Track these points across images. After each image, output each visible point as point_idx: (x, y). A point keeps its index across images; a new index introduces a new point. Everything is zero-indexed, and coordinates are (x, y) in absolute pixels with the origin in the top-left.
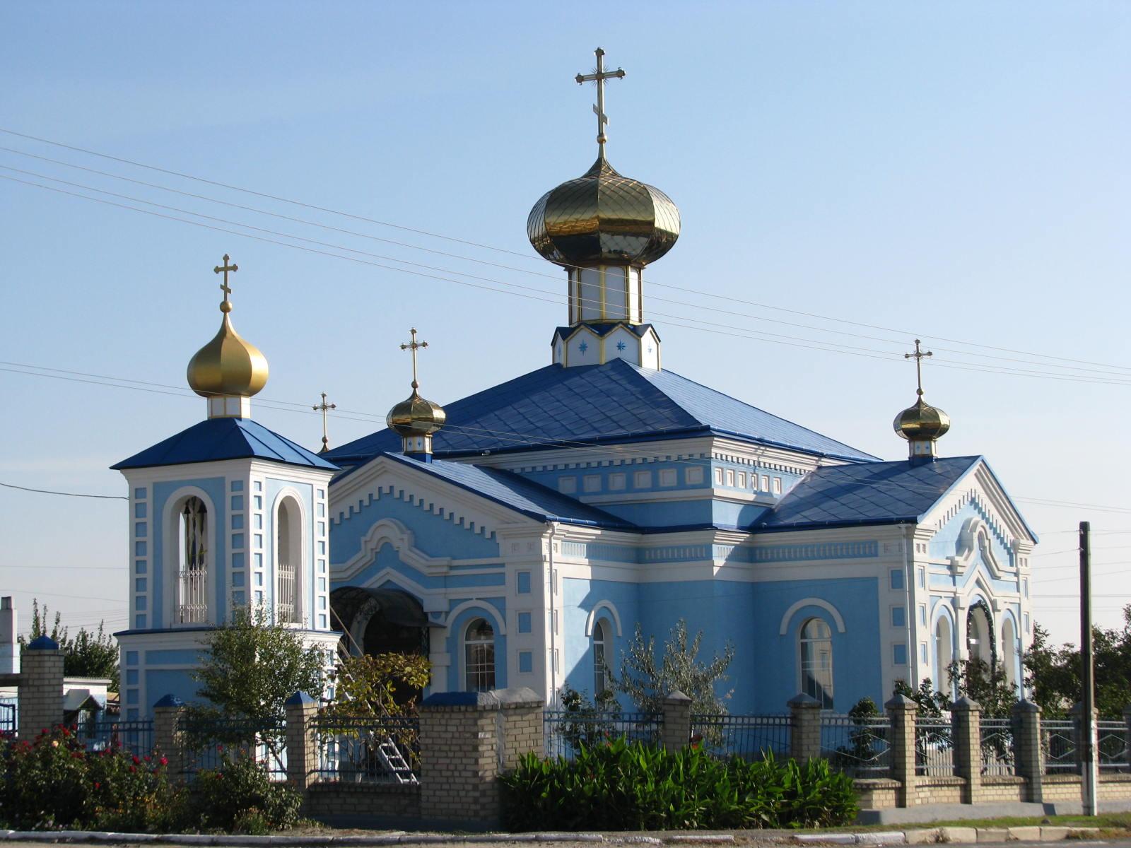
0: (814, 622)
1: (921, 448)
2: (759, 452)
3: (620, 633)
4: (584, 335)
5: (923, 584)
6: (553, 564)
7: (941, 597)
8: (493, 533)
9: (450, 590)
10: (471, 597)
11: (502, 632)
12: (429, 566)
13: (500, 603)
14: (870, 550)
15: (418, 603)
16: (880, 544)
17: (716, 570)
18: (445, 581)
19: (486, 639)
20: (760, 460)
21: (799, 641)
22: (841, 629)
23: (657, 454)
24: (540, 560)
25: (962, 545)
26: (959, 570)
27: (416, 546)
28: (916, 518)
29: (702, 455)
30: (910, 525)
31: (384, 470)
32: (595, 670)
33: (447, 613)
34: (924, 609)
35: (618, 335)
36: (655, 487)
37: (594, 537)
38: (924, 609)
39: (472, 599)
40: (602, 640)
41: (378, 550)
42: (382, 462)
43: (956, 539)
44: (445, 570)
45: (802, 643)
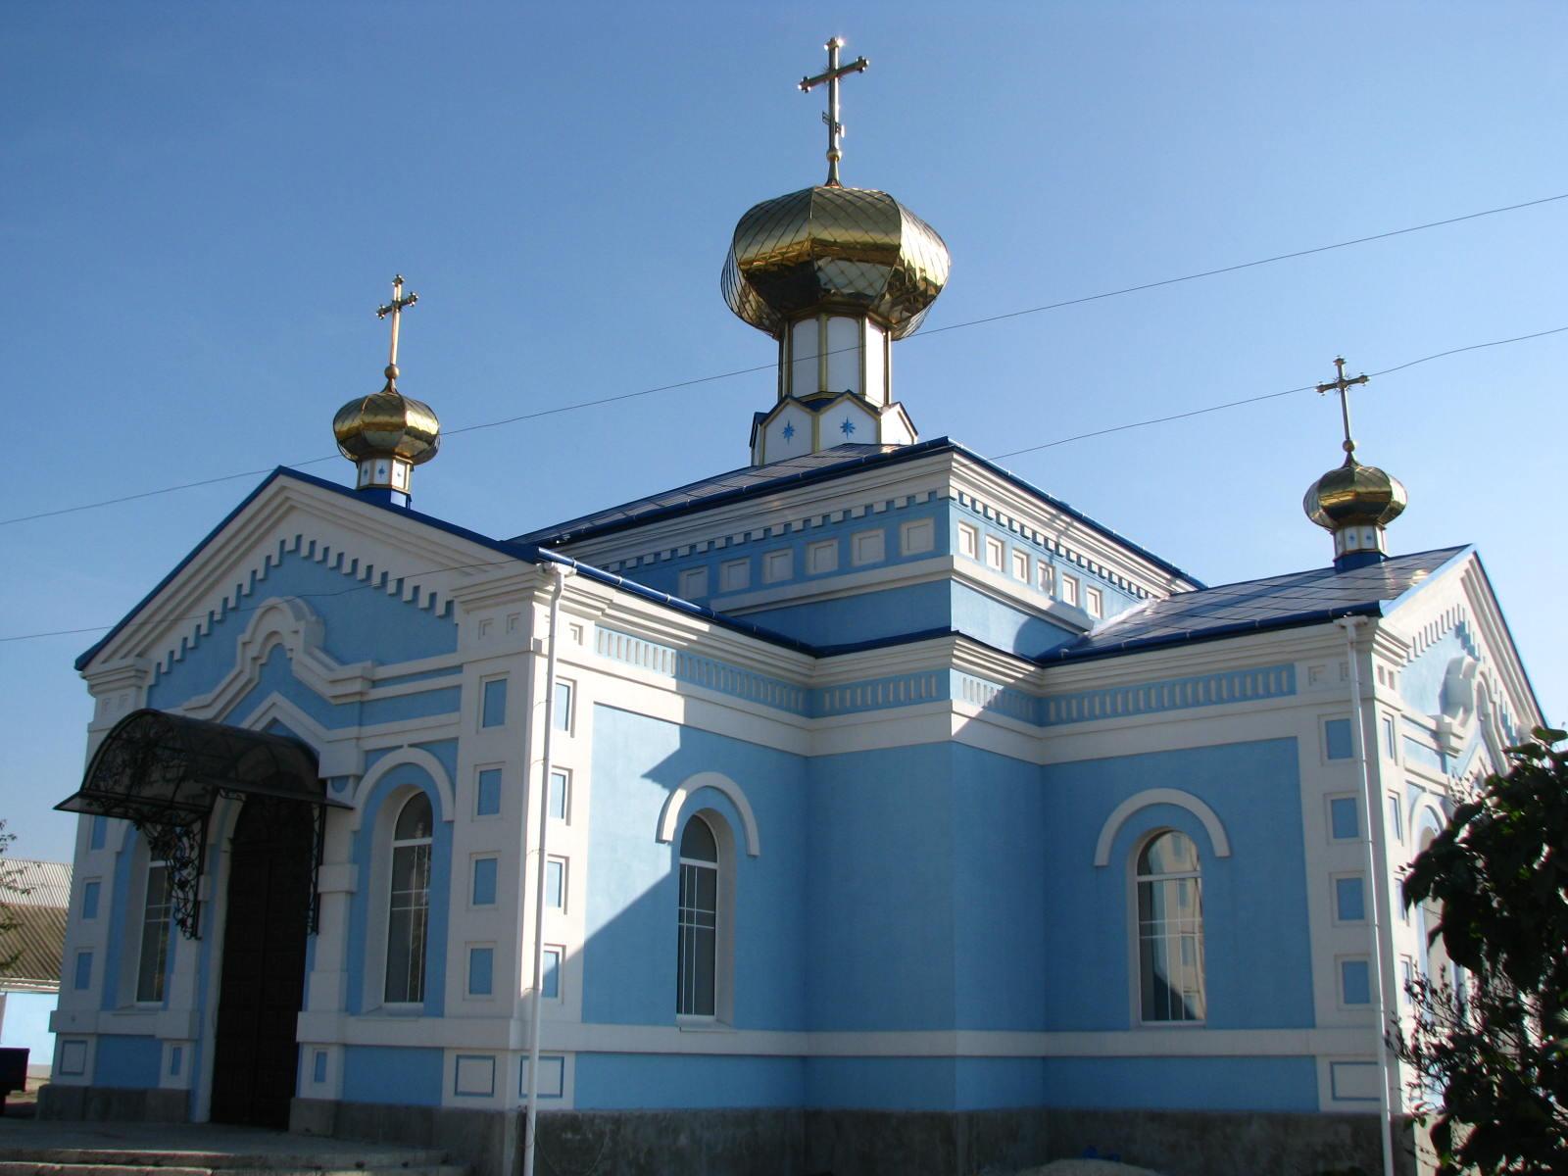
0: (1165, 844)
1: (1356, 538)
2: (1060, 525)
3: (755, 849)
4: (794, 415)
5: (1393, 753)
6: (556, 665)
7: (1424, 789)
8: (449, 604)
9: (368, 730)
10: (399, 744)
11: (447, 817)
12: (334, 682)
13: (445, 750)
14: (1278, 682)
15: (311, 757)
16: (1301, 670)
17: (957, 724)
18: (362, 710)
19: (1306, 1063)
20: (1062, 542)
21: (1134, 879)
22: (1221, 848)
23: (845, 503)
24: (525, 652)
25: (1450, 700)
26: (1454, 742)
27: (326, 650)
28: (1377, 603)
29: (932, 494)
30: (1364, 618)
31: (287, 505)
32: (681, 920)
33: (359, 778)
34: (1396, 802)
35: (843, 411)
36: (845, 567)
37: (694, 638)
38: (1396, 802)
39: (401, 747)
40: (715, 861)
41: (263, 661)
42: (283, 488)
43: (1438, 690)
44: (357, 686)
45: (1141, 885)
